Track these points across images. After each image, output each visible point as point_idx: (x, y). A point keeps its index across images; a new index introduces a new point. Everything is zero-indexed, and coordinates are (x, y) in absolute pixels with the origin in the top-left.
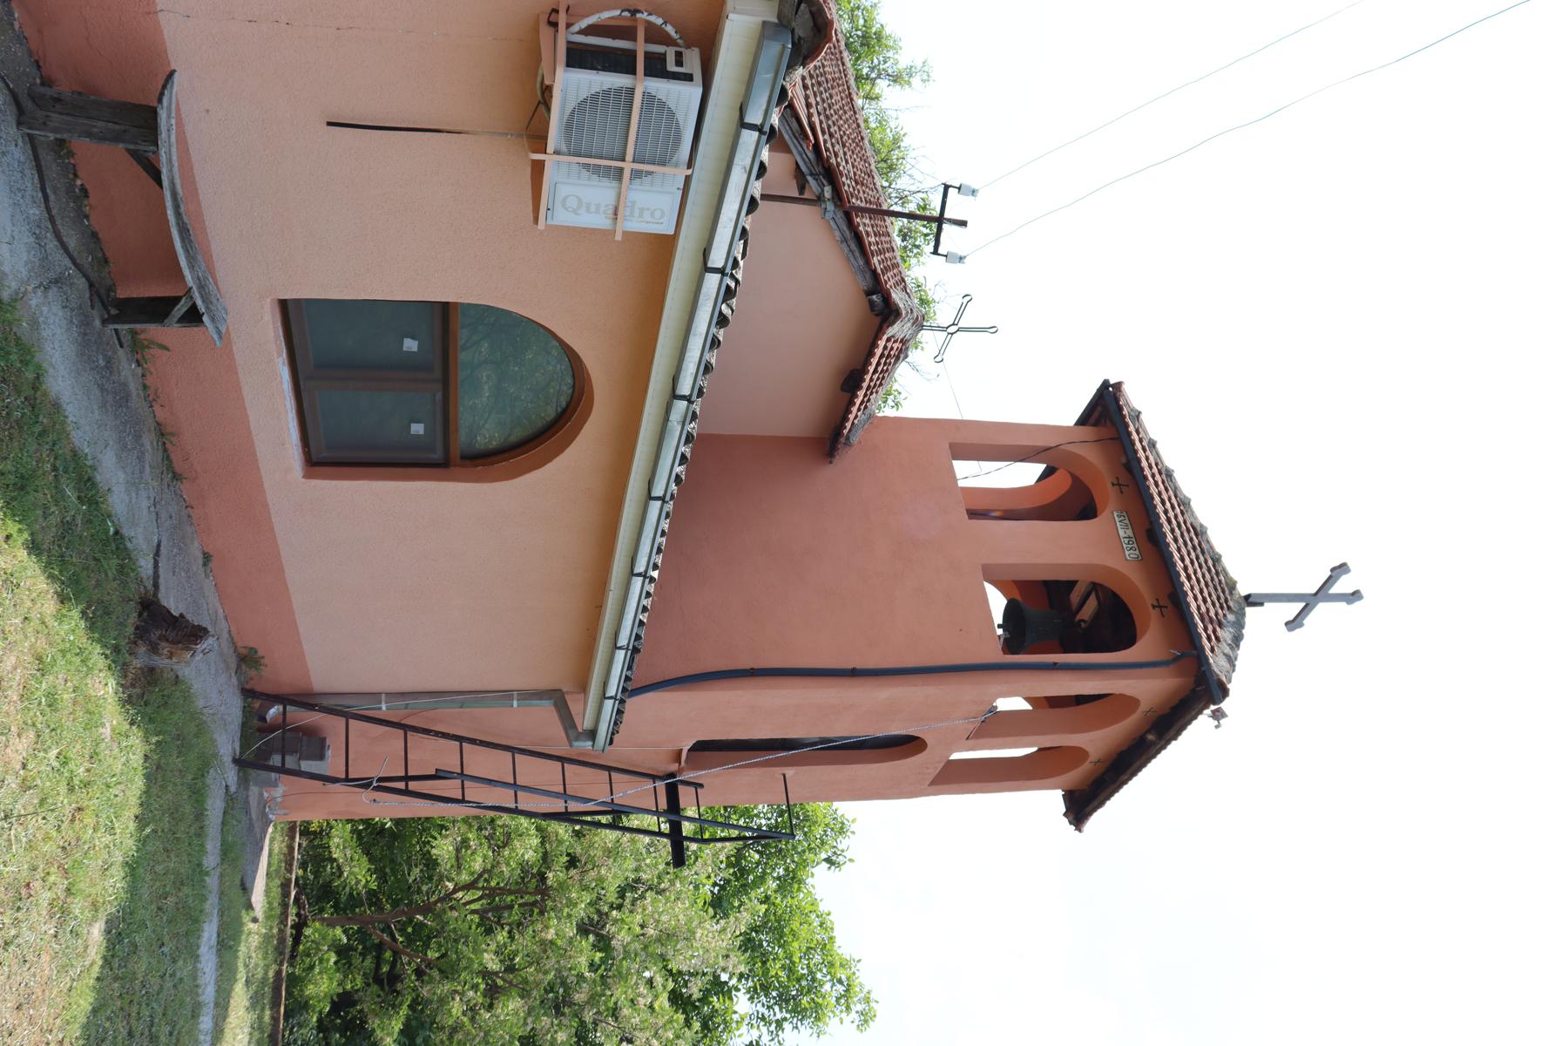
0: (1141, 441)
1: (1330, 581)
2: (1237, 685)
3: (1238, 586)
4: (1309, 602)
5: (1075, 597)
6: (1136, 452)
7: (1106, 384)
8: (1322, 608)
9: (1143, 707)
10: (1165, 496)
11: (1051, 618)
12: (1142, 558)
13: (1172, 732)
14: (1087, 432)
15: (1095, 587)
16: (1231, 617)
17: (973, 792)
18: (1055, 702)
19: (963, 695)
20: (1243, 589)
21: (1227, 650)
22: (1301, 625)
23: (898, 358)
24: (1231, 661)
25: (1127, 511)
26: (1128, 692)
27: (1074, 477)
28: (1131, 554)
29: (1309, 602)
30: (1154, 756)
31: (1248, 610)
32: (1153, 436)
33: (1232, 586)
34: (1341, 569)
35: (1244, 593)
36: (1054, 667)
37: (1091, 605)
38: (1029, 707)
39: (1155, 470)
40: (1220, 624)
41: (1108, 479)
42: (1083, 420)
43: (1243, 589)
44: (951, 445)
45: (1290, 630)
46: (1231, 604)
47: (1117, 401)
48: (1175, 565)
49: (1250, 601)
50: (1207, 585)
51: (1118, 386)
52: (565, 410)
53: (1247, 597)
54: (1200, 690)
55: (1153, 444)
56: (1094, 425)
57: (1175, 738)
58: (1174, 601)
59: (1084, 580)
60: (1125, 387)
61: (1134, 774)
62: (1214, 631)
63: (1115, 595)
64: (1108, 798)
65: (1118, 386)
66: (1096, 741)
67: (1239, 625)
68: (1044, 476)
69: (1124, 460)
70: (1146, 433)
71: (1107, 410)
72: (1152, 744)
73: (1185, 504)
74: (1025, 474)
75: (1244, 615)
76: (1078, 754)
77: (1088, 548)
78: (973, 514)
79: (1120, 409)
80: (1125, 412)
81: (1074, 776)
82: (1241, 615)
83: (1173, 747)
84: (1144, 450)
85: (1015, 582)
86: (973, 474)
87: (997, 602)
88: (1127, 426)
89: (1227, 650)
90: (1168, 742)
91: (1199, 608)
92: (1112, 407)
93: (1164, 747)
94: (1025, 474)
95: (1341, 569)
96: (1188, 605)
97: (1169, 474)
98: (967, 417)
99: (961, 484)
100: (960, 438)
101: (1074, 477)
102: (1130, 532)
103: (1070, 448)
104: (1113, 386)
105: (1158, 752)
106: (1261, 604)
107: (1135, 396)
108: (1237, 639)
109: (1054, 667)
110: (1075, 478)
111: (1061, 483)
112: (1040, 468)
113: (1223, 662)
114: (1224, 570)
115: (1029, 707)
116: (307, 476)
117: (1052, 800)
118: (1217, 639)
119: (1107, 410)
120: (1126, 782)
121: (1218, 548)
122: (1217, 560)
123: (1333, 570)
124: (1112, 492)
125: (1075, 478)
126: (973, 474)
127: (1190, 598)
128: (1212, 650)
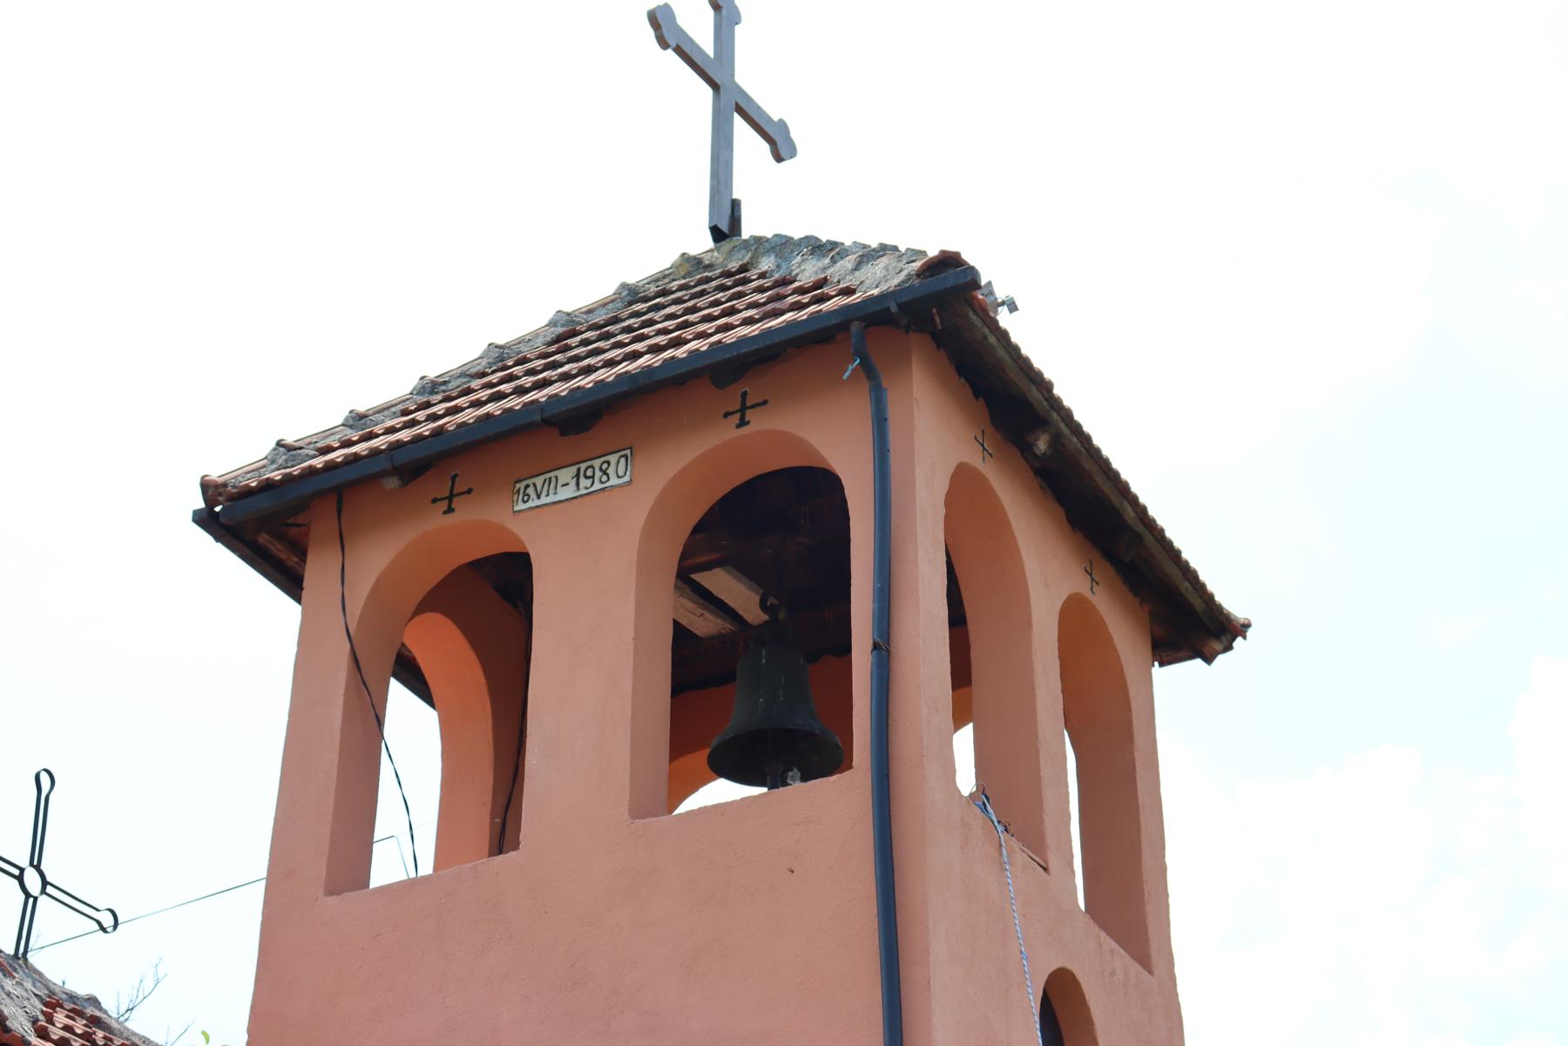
0: (347, 443)
1: (688, 54)
2: (932, 240)
3: (694, 251)
4: (732, 105)
5: (705, 624)
6: (375, 453)
7: (206, 520)
8: (748, 76)
9: (973, 457)
10: (484, 394)
11: (764, 673)
12: (629, 450)
13: (1034, 394)
14: (319, 569)
15: (685, 576)
16: (766, 264)
17: (1162, 869)
18: (961, 674)
19: (952, 870)
20: (701, 243)
21: (848, 263)
22: (782, 125)
23: (95, 1021)
24: (868, 255)
25: (515, 483)
26: (941, 485)
27: (425, 606)
28: (617, 471)
29: (732, 105)
30: (1086, 439)
31: (750, 227)
32: (338, 418)
33: (692, 263)
34: (662, 25)
35: (707, 242)
36: (883, 649)
37: (721, 582)
38: (970, 727)
39: (421, 415)
40: (784, 282)
41: (436, 521)
42: (290, 581)
43: (701, 243)
44: (332, 891)
45: (793, 152)
46: (734, 265)
47: (247, 493)
48: (649, 370)
49: (725, 229)
50: (694, 310)
51: (210, 489)
52: (818, 342)
53: (717, 234)
54: (943, 316)
55: (357, 419)
56: (302, 555)
57: (1047, 387)
58: (735, 375)
59: (668, 606)
60: (216, 472)
61: (1123, 489)
62: (802, 291)
63: (696, 530)
64: (1175, 555)
65: (210, 489)
66: (1048, 573)
67: (782, 246)
68: (421, 689)
69: (392, 483)
70: (330, 432)
71: (266, 520)
72: (1057, 441)
73: (502, 360)
74: (412, 729)
75: (758, 240)
76: (1075, 616)
77: (600, 572)
78: (503, 836)
79: (268, 486)
80: (276, 476)
81: (1124, 634)
82: (759, 245)
83: (1064, 391)
84: (371, 436)
85: (671, 760)
86: (407, 831)
87: (721, 791)
88: (312, 471)
89: (848, 263)
90: (1056, 404)
91: (749, 321)
92: (264, 503)
93: (1067, 415)
94: (412, 729)
95: (662, 25)
96: (743, 341)
97: (430, 387)
98: (261, 869)
99: (426, 868)
100: (316, 869)
101: (425, 606)
102: (566, 475)
103: (356, 607)
104: (210, 500)
105: (1076, 429)
106: (735, 205)
107: (241, 452)
108: (816, 247)
109: (883, 649)
110: (429, 603)
111: (440, 643)
112: (399, 696)
113: (876, 270)
114: (655, 280)
115: (970, 727)
116: (516, 846)
117: (1178, 691)
118: (822, 283)
119: (266, 520)
120: (1142, 511)
121: (607, 289)
122: (631, 294)
123: (664, 44)
124: (468, 513)
125: (429, 603)
126: (407, 831)
127: (729, 337)
128: (849, 291)
